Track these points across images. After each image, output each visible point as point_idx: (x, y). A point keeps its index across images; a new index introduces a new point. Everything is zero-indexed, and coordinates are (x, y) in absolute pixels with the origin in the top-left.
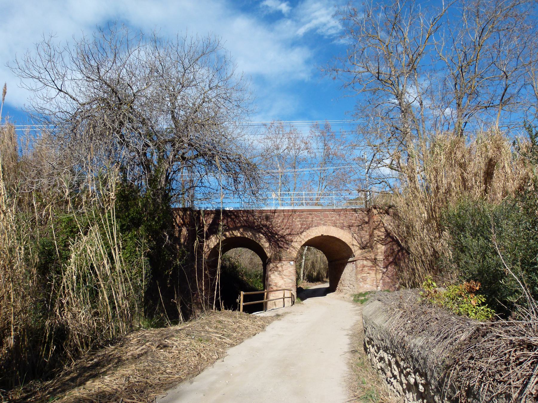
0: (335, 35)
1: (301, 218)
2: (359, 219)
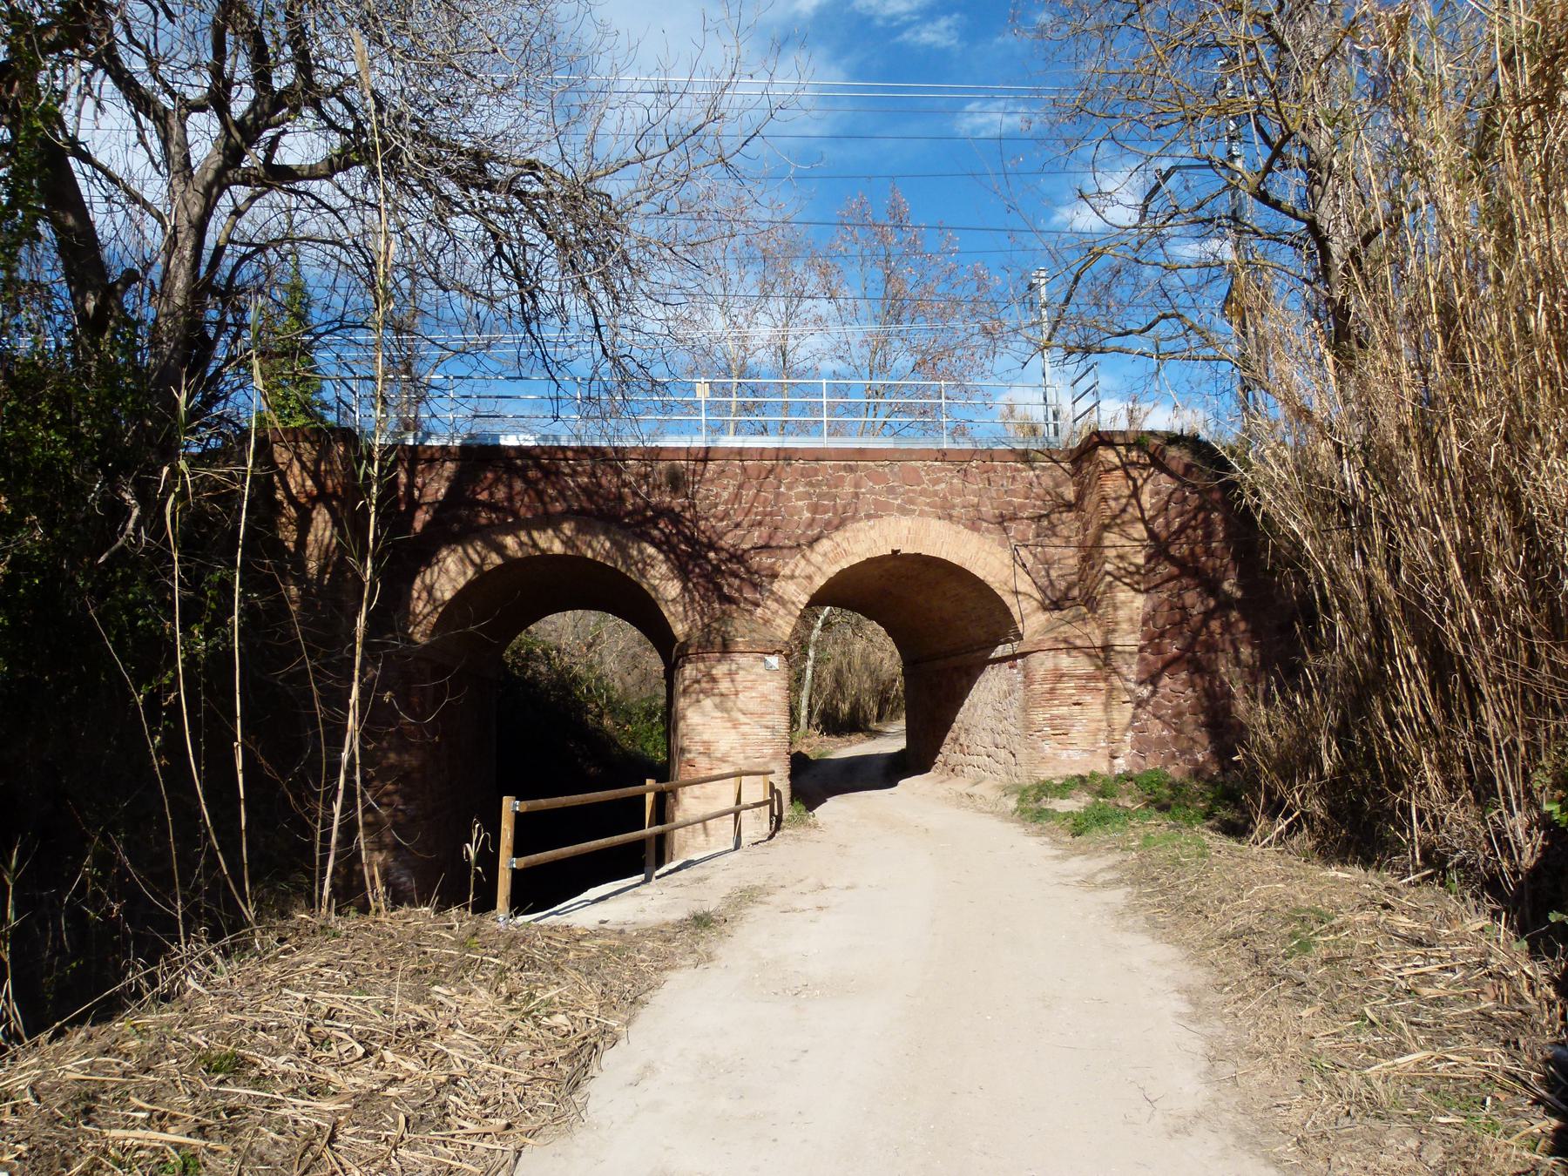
0: (906, 18)
1: (810, 484)
2: (1041, 492)
